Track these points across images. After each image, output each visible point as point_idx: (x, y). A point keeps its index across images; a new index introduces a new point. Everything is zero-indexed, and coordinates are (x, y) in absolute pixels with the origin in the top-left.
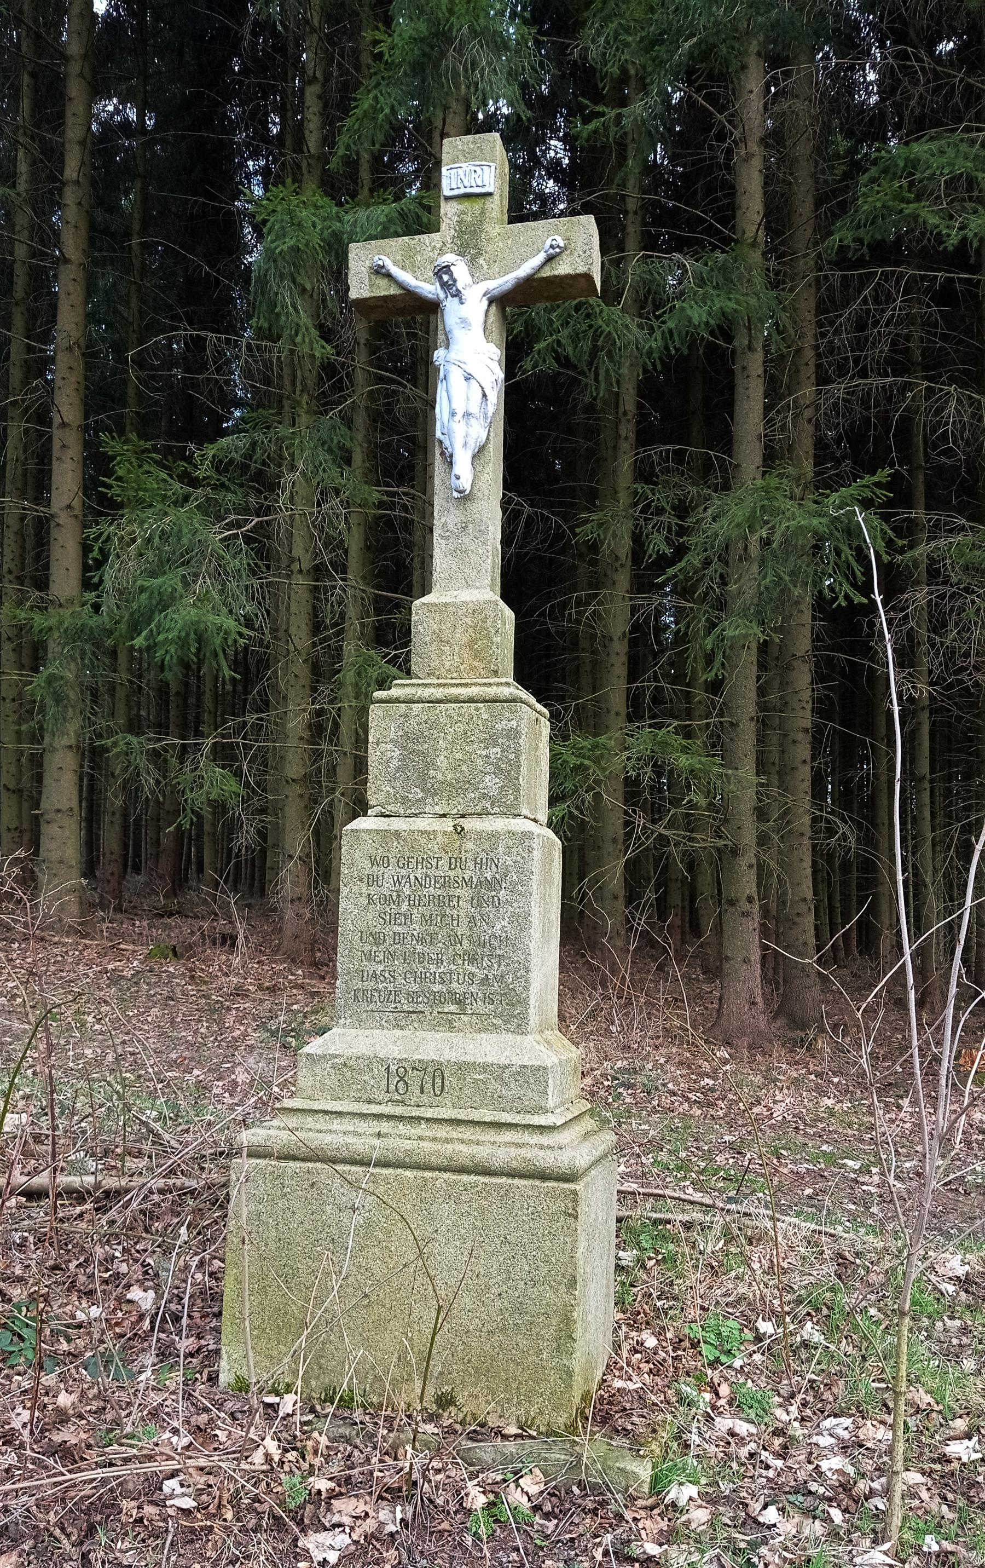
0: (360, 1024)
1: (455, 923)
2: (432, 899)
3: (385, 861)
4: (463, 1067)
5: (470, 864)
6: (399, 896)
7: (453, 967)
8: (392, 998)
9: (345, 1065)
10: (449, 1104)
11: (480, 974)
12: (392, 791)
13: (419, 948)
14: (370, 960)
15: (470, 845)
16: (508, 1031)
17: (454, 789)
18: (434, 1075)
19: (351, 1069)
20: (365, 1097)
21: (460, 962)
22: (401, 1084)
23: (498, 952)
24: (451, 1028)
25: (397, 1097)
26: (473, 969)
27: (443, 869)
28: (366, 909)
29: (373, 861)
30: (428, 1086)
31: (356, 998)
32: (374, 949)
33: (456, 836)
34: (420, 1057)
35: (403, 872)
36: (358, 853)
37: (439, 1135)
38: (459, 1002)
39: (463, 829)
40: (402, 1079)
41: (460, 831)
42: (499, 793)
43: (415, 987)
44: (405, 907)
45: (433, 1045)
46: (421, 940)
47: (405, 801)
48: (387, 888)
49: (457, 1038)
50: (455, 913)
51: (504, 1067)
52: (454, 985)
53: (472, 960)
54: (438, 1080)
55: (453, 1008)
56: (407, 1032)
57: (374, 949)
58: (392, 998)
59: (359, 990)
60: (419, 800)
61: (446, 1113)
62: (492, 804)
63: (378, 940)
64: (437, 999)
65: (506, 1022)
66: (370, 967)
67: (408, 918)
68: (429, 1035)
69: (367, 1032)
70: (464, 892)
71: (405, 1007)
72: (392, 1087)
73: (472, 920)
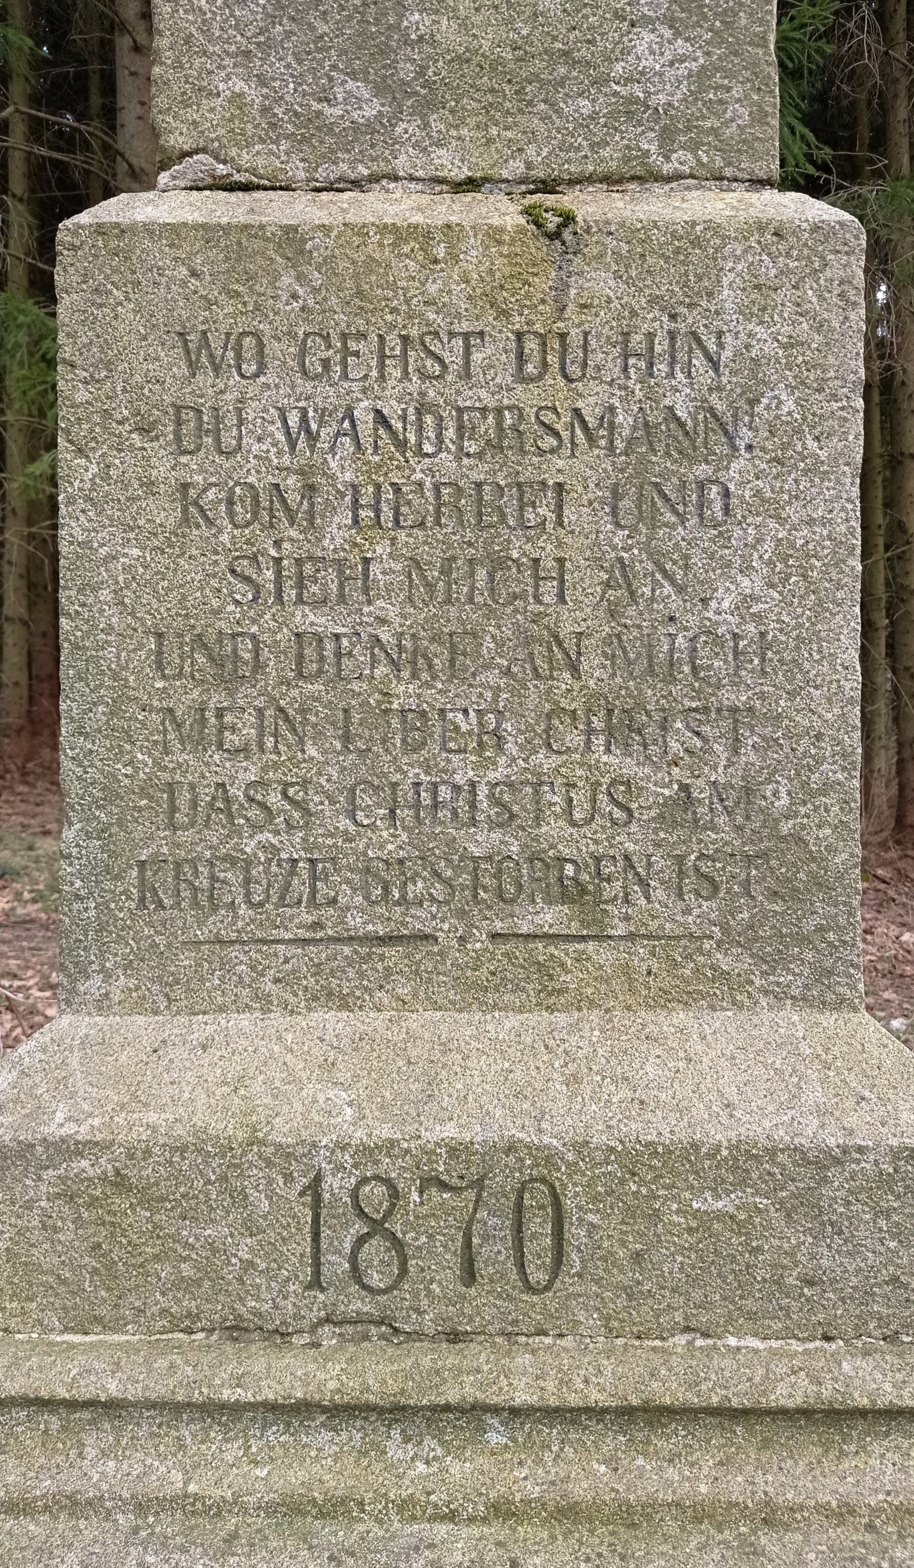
0: (173, 992)
1: (549, 589)
2: (447, 499)
3: (246, 352)
4: (649, 1169)
5: (606, 358)
6: (310, 489)
7: (545, 761)
8: (300, 886)
9: (120, 1182)
10: (590, 1321)
11: (659, 787)
12: (254, 94)
13: (404, 692)
14: (199, 743)
15: (600, 282)
16: (780, 996)
17: (515, 83)
18: (521, 1218)
19: (149, 1198)
20: (217, 1311)
21: (574, 739)
22: (375, 1250)
23: (728, 696)
24: (550, 996)
25: (360, 1305)
26: (630, 767)
27: (492, 378)
28: (173, 542)
29: (196, 352)
30: (494, 1253)
31: (147, 895)
32: (217, 699)
33: (539, 248)
34: (449, 1131)
35: (327, 394)
36: (129, 320)
37: (580, 1490)
38: (573, 894)
39: (568, 219)
40: (377, 1227)
41: (559, 232)
42: (694, 96)
43: (391, 843)
44: (337, 532)
45: (495, 1075)
46: (410, 659)
47: (310, 130)
48: (262, 456)
49: (583, 1034)
50: (547, 551)
51: (823, 1162)
52: (553, 828)
53: (623, 728)
54: (539, 1227)
55: (551, 917)
56: (374, 1021)
57: (217, 699)
58: (300, 886)
59: (159, 861)
60: (369, 127)
61: (602, 1379)
62: (667, 138)
63: (228, 667)
64: (486, 886)
65: (772, 963)
66: (204, 770)
67: (355, 577)
68: (463, 1026)
69: (204, 1027)
70: (583, 470)
71: (355, 921)
72: (336, 1264)
73: (621, 575)
